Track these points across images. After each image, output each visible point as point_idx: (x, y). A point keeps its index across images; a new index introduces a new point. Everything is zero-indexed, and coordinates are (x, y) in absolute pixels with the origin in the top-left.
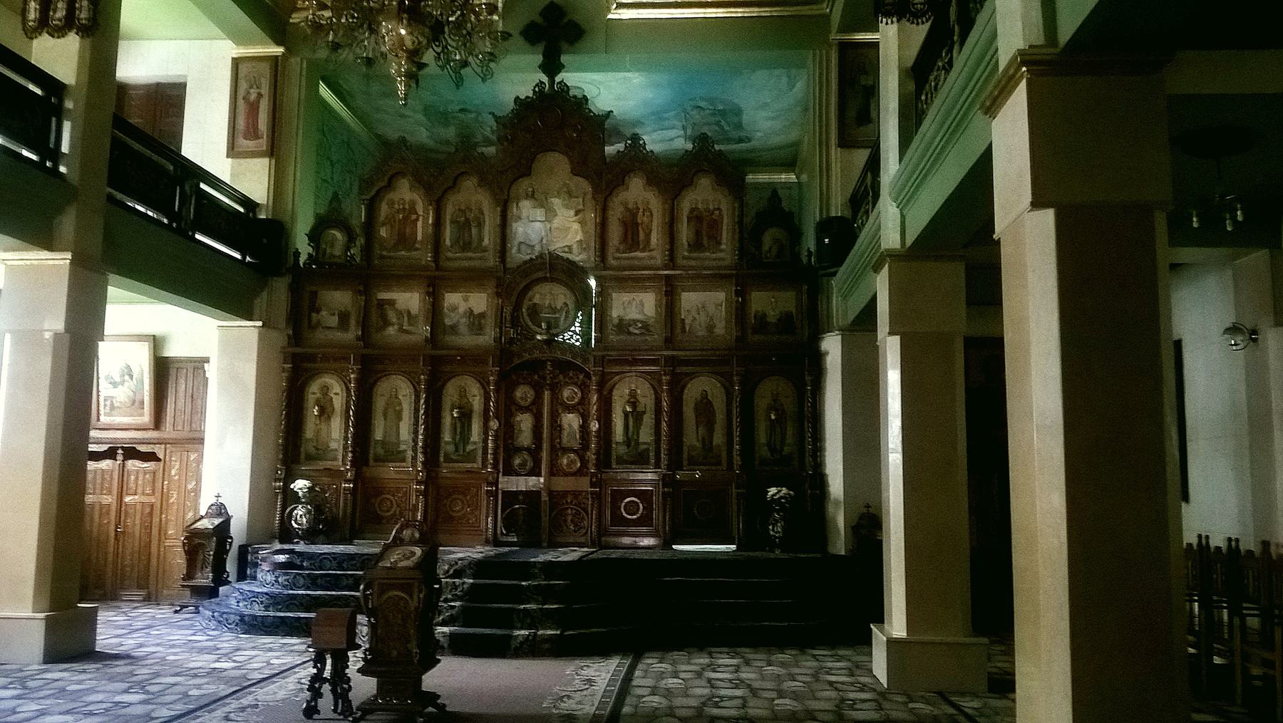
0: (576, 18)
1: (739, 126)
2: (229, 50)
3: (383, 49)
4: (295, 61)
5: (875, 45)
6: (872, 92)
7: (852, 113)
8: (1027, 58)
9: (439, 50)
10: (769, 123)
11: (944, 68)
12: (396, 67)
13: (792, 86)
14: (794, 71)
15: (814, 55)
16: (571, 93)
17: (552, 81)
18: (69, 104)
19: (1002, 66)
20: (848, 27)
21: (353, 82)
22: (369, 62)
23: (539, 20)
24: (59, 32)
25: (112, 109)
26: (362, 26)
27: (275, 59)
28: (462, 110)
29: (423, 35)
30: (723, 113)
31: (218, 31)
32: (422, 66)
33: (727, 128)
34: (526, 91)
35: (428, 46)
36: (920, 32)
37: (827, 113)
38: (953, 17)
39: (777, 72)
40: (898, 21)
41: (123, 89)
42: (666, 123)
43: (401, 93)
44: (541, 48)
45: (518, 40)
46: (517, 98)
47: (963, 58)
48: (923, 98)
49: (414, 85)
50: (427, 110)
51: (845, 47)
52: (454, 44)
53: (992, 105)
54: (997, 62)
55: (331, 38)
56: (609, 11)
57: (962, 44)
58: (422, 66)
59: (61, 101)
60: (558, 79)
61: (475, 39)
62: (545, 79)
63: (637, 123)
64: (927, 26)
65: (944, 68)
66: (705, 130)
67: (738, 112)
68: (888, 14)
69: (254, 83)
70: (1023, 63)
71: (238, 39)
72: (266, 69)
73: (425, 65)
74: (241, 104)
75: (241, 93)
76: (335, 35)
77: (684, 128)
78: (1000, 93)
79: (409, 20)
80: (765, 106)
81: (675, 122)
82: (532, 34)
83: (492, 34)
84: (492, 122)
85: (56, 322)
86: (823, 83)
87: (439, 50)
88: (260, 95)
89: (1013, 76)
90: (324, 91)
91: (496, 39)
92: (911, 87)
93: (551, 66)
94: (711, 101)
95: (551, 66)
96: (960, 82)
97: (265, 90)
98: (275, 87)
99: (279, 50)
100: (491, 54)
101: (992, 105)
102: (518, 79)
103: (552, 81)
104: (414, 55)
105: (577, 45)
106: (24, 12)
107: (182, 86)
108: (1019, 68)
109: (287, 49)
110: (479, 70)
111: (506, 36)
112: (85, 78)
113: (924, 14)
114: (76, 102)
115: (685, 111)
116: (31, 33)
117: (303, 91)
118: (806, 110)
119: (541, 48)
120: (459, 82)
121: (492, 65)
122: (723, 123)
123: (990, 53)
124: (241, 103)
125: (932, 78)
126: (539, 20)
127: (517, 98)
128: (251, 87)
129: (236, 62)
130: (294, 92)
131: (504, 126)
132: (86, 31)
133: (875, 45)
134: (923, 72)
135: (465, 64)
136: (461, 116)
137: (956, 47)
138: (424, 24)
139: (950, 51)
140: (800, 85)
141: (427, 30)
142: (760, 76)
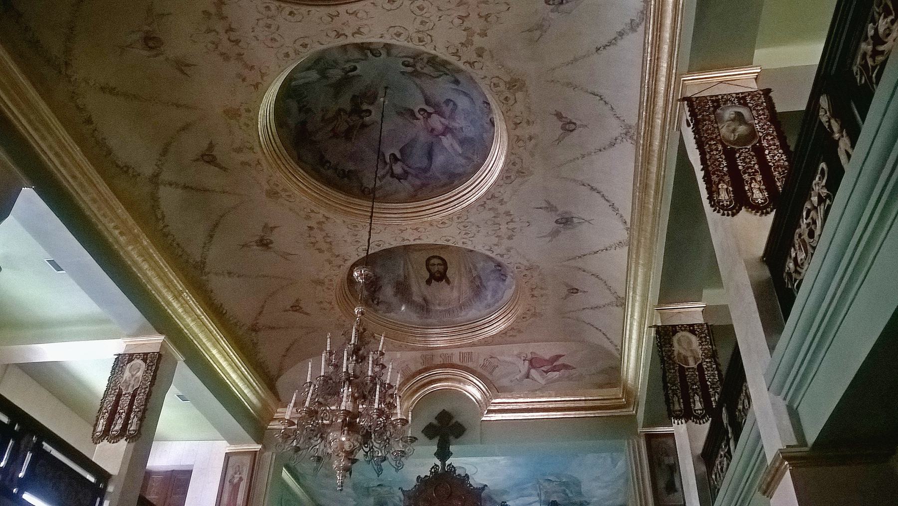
0: (460, 420)
1: (580, 493)
2: (224, 447)
3: (330, 451)
4: (268, 454)
5: (672, 435)
6: (674, 469)
7: (662, 484)
8: (787, 455)
9: (367, 450)
10: (600, 491)
11: (725, 456)
12: (338, 463)
13: (614, 463)
14: (615, 454)
15: (628, 443)
16: (457, 472)
17: (444, 464)
18: (110, 489)
19: (769, 460)
20: (651, 421)
21: (306, 467)
22: (319, 459)
23: (435, 422)
24: (116, 439)
25: (137, 493)
26: (316, 436)
27: (255, 453)
28: (379, 485)
29: (357, 440)
30: (566, 484)
31: (218, 435)
32: (354, 461)
33: (570, 495)
34: (425, 472)
35: (360, 448)
36: (704, 428)
37: (642, 473)
38: (725, 421)
39: (603, 455)
40: (686, 422)
41: (148, 474)
42: (525, 492)
43: (339, 482)
44: (436, 440)
45: (422, 437)
46: (419, 477)
47: (740, 450)
48: (714, 477)
49: (348, 474)
50: (355, 487)
51: (649, 437)
52: (377, 446)
53: (768, 487)
54: (765, 455)
55: (294, 444)
56: (482, 414)
57: (736, 441)
58: (354, 461)
59: (106, 487)
60: (448, 462)
61: (392, 442)
62: (439, 463)
63: (504, 492)
64: (707, 425)
65: (725, 456)
66: (554, 498)
67: (578, 484)
68: (678, 417)
69: (238, 470)
70: (785, 458)
71: (231, 441)
72: (247, 460)
73: (357, 460)
74: (228, 487)
75: (228, 477)
76: (298, 443)
77: (539, 495)
78: (772, 479)
79: (348, 431)
80: (597, 479)
81: (534, 492)
82: (430, 431)
83: (405, 440)
84: (400, 493)
85: (46, 393)
86: (638, 464)
87: (367, 450)
88: (241, 479)
89: (777, 470)
90: (285, 475)
91: (406, 442)
92: (704, 468)
93: (443, 453)
94: (558, 476)
95: (443, 453)
96: (739, 468)
97: (245, 476)
98: (253, 471)
99: (258, 447)
100: (403, 452)
101: (768, 487)
102: (422, 462)
103: (444, 464)
104: (350, 456)
105: (460, 439)
106: (96, 425)
107: (190, 472)
108: (782, 463)
109: (264, 447)
110: (394, 463)
111: (414, 439)
112: (125, 472)
113: (703, 417)
114: (116, 486)
115: (538, 482)
116: (96, 440)
117: (271, 476)
118: (627, 480)
119: (436, 440)
120: (379, 471)
121: (403, 459)
122: (567, 491)
123: (761, 456)
124: (227, 484)
125: (717, 462)
126: (435, 422)
127: (419, 477)
128: (236, 473)
129: (228, 456)
130: (265, 475)
131: (409, 498)
132: (131, 438)
133: (672, 435)
134: (711, 456)
135: (384, 459)
136: (379, 489)
137: (732, 443)
138: (358, 433)
139: (728, 444)
140: (621, 463)
141: (360, 437)
142: (590, 458)
